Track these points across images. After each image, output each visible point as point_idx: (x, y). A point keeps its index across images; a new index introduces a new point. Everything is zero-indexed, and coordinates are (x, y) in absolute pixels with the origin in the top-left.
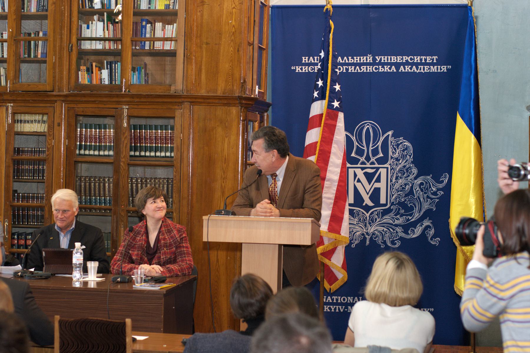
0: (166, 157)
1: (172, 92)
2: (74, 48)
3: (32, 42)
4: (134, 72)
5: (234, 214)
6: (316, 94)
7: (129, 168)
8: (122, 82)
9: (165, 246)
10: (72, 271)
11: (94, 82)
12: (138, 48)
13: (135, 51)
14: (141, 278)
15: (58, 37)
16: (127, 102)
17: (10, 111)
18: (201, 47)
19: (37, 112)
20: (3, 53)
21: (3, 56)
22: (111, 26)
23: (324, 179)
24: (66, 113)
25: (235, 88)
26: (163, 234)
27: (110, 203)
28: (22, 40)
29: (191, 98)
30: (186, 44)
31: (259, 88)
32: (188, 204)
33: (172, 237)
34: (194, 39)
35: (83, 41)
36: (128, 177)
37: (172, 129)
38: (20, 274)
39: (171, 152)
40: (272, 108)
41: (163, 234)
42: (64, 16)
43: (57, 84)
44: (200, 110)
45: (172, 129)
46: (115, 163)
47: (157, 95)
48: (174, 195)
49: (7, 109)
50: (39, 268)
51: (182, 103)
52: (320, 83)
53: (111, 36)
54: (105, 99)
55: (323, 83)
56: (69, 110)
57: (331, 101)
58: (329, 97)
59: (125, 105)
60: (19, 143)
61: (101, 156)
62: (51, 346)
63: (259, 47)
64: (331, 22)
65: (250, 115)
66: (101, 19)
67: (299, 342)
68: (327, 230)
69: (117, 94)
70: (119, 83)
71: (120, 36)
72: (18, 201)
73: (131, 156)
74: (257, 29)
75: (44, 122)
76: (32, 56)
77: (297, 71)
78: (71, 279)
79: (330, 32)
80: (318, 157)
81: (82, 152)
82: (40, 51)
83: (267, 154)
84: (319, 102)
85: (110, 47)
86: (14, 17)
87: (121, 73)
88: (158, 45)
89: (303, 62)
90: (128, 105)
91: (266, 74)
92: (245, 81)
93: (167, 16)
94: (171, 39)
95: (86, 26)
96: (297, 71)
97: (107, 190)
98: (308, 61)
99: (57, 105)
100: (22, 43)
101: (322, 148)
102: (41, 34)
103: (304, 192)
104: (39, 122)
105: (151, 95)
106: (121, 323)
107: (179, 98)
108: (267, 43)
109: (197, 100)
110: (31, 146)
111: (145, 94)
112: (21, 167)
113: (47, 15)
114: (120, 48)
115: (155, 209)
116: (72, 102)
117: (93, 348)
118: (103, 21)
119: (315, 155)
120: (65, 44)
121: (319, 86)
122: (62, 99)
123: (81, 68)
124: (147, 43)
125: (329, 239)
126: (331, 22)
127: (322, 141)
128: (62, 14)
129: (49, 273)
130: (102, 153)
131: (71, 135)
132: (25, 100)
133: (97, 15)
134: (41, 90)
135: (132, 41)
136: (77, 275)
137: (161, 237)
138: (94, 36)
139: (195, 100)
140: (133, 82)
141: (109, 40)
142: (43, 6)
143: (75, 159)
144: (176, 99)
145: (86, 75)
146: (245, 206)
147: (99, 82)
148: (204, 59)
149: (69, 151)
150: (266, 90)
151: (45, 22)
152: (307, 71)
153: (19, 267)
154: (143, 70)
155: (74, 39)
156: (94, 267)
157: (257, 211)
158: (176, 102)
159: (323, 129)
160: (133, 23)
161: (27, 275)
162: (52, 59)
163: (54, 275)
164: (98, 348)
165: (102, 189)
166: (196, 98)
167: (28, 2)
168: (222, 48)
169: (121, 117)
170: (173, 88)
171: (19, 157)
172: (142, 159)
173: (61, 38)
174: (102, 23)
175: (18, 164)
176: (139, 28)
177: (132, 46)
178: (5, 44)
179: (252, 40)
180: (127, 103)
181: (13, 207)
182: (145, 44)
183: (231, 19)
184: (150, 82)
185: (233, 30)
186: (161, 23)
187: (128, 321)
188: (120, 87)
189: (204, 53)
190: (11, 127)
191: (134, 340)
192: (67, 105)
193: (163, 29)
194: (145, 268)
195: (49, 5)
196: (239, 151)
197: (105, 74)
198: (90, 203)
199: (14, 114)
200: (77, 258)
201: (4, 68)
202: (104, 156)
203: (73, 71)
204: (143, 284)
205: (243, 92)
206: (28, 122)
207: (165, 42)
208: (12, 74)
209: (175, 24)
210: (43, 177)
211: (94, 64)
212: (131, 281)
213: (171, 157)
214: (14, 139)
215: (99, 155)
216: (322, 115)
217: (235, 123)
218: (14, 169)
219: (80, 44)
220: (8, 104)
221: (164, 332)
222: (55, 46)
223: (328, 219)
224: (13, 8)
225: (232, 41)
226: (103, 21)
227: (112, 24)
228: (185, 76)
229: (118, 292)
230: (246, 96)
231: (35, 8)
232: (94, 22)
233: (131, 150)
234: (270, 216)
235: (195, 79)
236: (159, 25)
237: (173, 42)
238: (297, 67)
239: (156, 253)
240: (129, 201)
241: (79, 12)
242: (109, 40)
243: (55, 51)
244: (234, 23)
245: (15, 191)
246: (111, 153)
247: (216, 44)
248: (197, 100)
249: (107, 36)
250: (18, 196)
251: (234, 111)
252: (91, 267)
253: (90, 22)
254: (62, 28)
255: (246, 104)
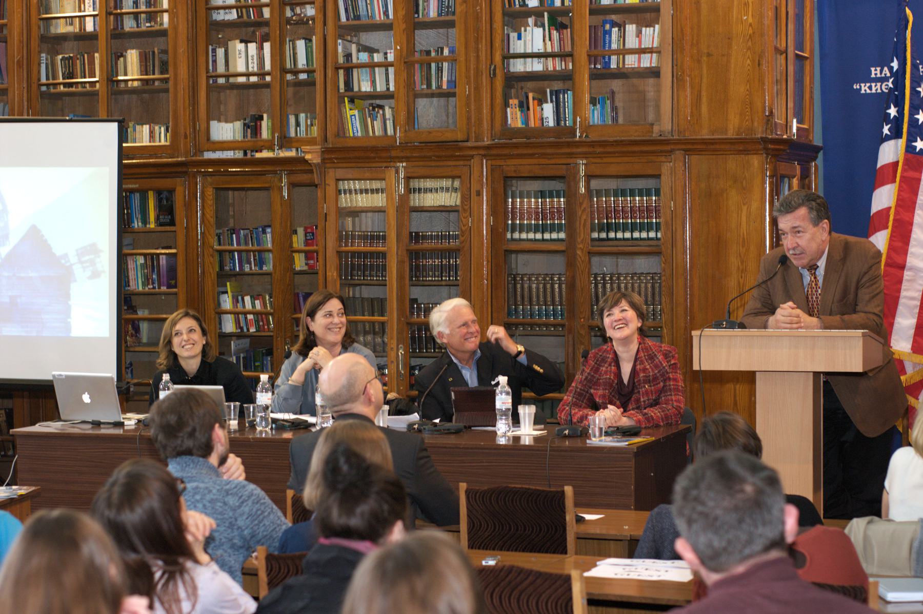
0: (648, 239)
1: (655, 135)
2: (498, 71)
3: (433, 65)
4: (595, 105)
5: (742, 326)
6: (886, 130)
7: (590, 261)
8: (575, 122)
9: (647, 381)
10: (496, 420)
11: (532, 124)
12: (599, 66)
13: (595, 71)
14: (601, 429)
15: (472, 55)
16: (585, 153)
17: (402, 175)
18: (699, 61)
19: (444, 174)
20: (388, 84)
21: (388, 89)
22: (555, 34)
23: (902, 267)
24: (489, 174)
25: (756, 124)
26: (642, 363)
27: (562, 315)
28: (417, 62)
29: (685, 144)
30: (675, 56)
31: (798, 122)
32: (686, 314)
33: (656, 366)
34: (687, 47)
35: (511, 60)
36: (589, 274)
37: (658, 193)
38: (416, 427)
39: (657, 231)
40: (824, 154)
41: (642, 363)
42: (481, 21)
43: (473, 129)
44: (700, 163)
45: (658, 193)
46: (567, 251)
47: (631, 141)
48: (663, 300)
49: (397, 172)
50: (447, 418)
51: (672, 151)
52: (893, 111)
53: (556, 49)
54: (549, 151)
55: (897, 112)
56: (493, 170)
57: (911, 139)
58: (909, 133)
59: (582, 158)
60: (418, 224)
61: (547, 240)
62: (454, 527)
63: (797, 55)
64: (908, 11)
65: (783, 168)
66: (539, 23)
67: (742, 491)
68: (910, 351)
69: (568, 142)
70: (571, 124)
71: (570, 49)
72: (418, 315)
73: (593, 240)
74: (791, 27)
75: (456, 190)
76: (434, 87)
77: (863, 92)
78: (495, 433)
79: (906, 28)
80: (892, 232)
81: (516, 235)
82: (445, 79)
83: (815, 229)
84: (892, 143)
85: (554, 68)
86: (404, 26)
87: (574, 107)
88: (631, 61)
89: (873, 76)
90: (586, 158)
91: (812, 98)
92: (771, 113)
93: (645, 15)
94: (650, 51)
95: (515, 35)
96: (863, 92)
97: (557, 294)
98: (881, 73)
99: (475, 162)
100: (417, 66)
101: (898, 217)
102: (446, 52)
103: (857, 288)
104: (447, 190)
105: (622, 141)
106: (557, 492)
107: (668, 144)
108: (812, 47)
109: (695, 147)
110: (436, 229)
111: (611, 139)
112: (422, 262)
113: (454, 21)
114: (571, 67)
115: (621, 323)
116: (499, 156)
117: (517, 530)
118: (543, 26)
119: (887, 228)
120: (483, 66)
121: (892, 117)
122: (482, 152)
123: (511, 101)
124: (614, 58)
125: (915, 365)
126: (908, 11)
127: (898, 205)
128: (478, 18)
129: (461, 425)
130: (547, 236)
131: (499, 210)
132: (425, 157)
133: (533, 17)
134: (449, 139)
135: (589, 56)
136: (502, 427)
137: (638, 367)
138: (529, 51)
139: (693, 147)
140: (594, 121)
141: (553, 55)
142: (448, 7)
143: (505, 247)
144: (655, 148)
145: (519, 113)
146: (757, 314)
147: (538, 124)
148: (705, 80)
149: (496, 234)
150: (812, 125)
151: (452, 31)
152: (879, 91)
153: (415, 417)
154: (608, 102)
155: (498, 58)
156: (530, 414)
157: (777, 321)
158: (661, 152)
159: (900, 186)
160: (590, 27)
161: (426, 427)
162: (464, 89)
163: (470, 427)
164: (525, 530)
165: (549, 294)
166: (693, 144)
167: (424, 1)
168: (733, 61)
169: (575, 178)
170: (656, 129)
171: (419, 246)
172: (610, 243)
173: (478, 57)
174: (541, 29)
175: (417, 258)
176: (600, 33)
177: (590, 64)
178: (391, 70)
179: (784, 45)
180: (584, 155)
181: (410, 324)
182: (609, 59)
183: (747, 14)
184: (621, 120)
185: (751, 31)
186: (634, 26)
187: (569, 490)
188: (572, 131)
189: (705, 71)
190: (404, 199)
191: (580, 520)
192: (489, 162)
193: (639, 34)
194: (609, 415)
195: (458, 6)
196: (765, 229)
197: (548, 109)
198: (532, 315)
199: (408, 179)
200: (503, 401)
201: (390, 107)
202: (552, 240)
203: (498, 109)
204: (603, 438)
205: (769, 131)
206: (431, 191)
207: (642, 55)
208: (403, 115)
209: (657, 26)
210: (456, 275)
211: (531, 95)
212: (585, 434)
213: (657, 239)
214: (410, 219)
215: (543, 240)
216: (897, 162)
217: (757, 182)
218: (411, 265)
219: (508, 65)
220: (398, 164)
221: (636, 509)
222: (468, 69)
223: (912, 332)
224: (402, 13)
225: (749, 49)
226: (543, 26)
227: (557, 29)
228: (675, 110)
229: (566, 451)
230: (774, 136)
231: (436, 10)
232: (528, 28)
233: (593, 230)
234: (797, 328)
235: (692, 112)
236: (631, 29)
237: (655, 55)
238: (863, 85)
239: (632, 392)
240: (592, 312)
241: (505, 14)
242: (553, 55)
243: (468, 77)
244: (750, 20)
245: (414, 301)
246: (562, 235)
247: (723, 55)
248: (695, 147)
249: (549, 50)
250: (419, 308)
251: (756, 161)
252: (524, 414)
253: (523, 29)
254: (477, 40)
255: (773, 150)
